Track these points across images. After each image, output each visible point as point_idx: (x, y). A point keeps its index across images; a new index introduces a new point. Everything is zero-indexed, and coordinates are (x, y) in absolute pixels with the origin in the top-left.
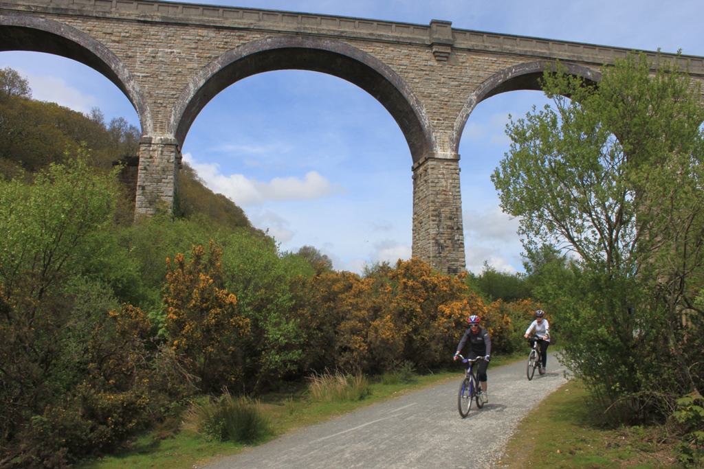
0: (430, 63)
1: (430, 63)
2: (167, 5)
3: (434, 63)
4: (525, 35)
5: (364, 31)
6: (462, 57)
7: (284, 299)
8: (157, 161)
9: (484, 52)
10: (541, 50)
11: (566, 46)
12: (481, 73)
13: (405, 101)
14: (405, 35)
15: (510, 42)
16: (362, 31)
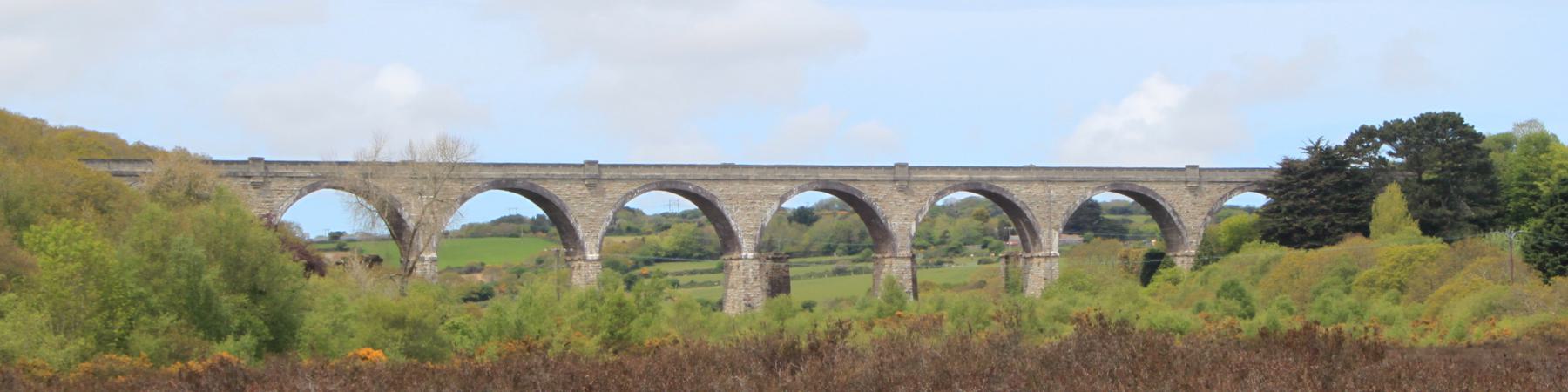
0: (584, 192)
1: (584, 192)
2: (1170, 176)
3: (586, 191)
4: (669, 163)
5: (543, 173)
6: (605, 185)
7: (804, 344)
8: (428, 271)
9: (620, 179)
10: (658, 173)
11: (675, 168)
12: (616, 195)
13: (568, 220)
14: (568, 173)
15: (794, 170)
16: (983, 176)
